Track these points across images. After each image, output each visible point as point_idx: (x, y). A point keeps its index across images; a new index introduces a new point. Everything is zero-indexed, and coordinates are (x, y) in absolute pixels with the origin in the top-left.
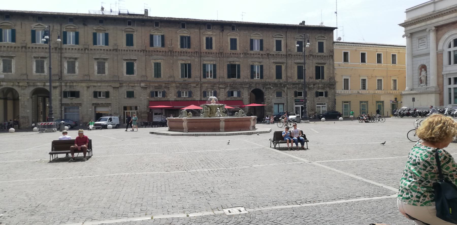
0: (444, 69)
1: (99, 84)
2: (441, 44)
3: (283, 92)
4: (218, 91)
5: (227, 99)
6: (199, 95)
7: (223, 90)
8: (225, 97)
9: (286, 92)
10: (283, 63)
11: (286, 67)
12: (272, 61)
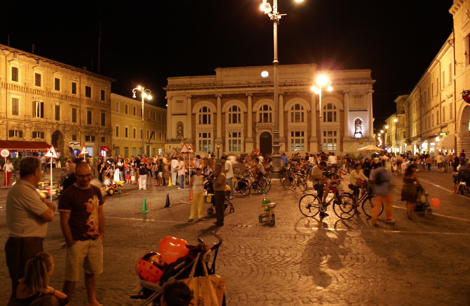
0: (226, 125)
1: (233, 86)
2: (255, 106)
3: (77, 136)
4: (24, 131)
5: (32, 140)
6: (5, 134)
7: (29, 129)
8: (31, 138)
9: (79, 135)
10: (77, 106)
11: (80, 111)
12: (70, 103)
